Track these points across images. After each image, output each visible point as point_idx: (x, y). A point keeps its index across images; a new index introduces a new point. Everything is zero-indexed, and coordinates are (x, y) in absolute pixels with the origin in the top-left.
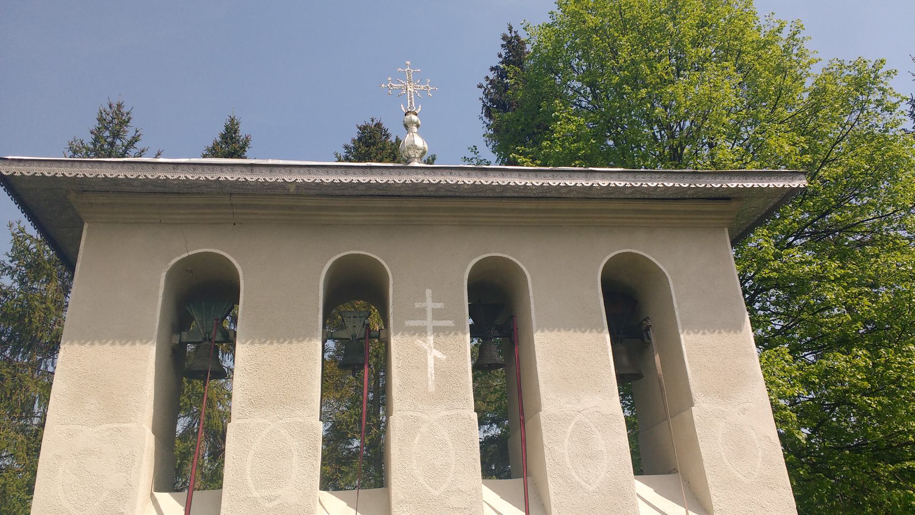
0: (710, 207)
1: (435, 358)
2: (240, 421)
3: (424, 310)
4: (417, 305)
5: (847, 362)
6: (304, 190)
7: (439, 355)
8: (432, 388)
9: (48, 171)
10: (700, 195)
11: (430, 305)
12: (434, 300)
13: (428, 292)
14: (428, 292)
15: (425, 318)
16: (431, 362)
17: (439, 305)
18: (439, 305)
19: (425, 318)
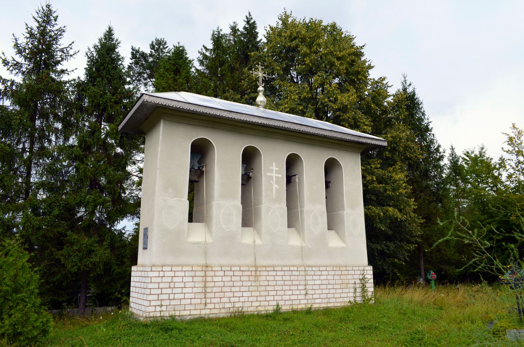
0: (358, 146)
1: (273, 181)
2: (217, 202)
3: (272, 170)
4: (271, 168)
5: (430, 231)
6: (325, 137)
7: (277, 186)
8: (274, 197)
9: (218, 113)
10: (283, 128)
11: (274, 168)
12: (276, 167)
13: (274, 164)
14: (274, 164)
15: (273, 173)
16: (274, 189)
17: (277, 169)
18: (277, 169)
19: (273, 173)
